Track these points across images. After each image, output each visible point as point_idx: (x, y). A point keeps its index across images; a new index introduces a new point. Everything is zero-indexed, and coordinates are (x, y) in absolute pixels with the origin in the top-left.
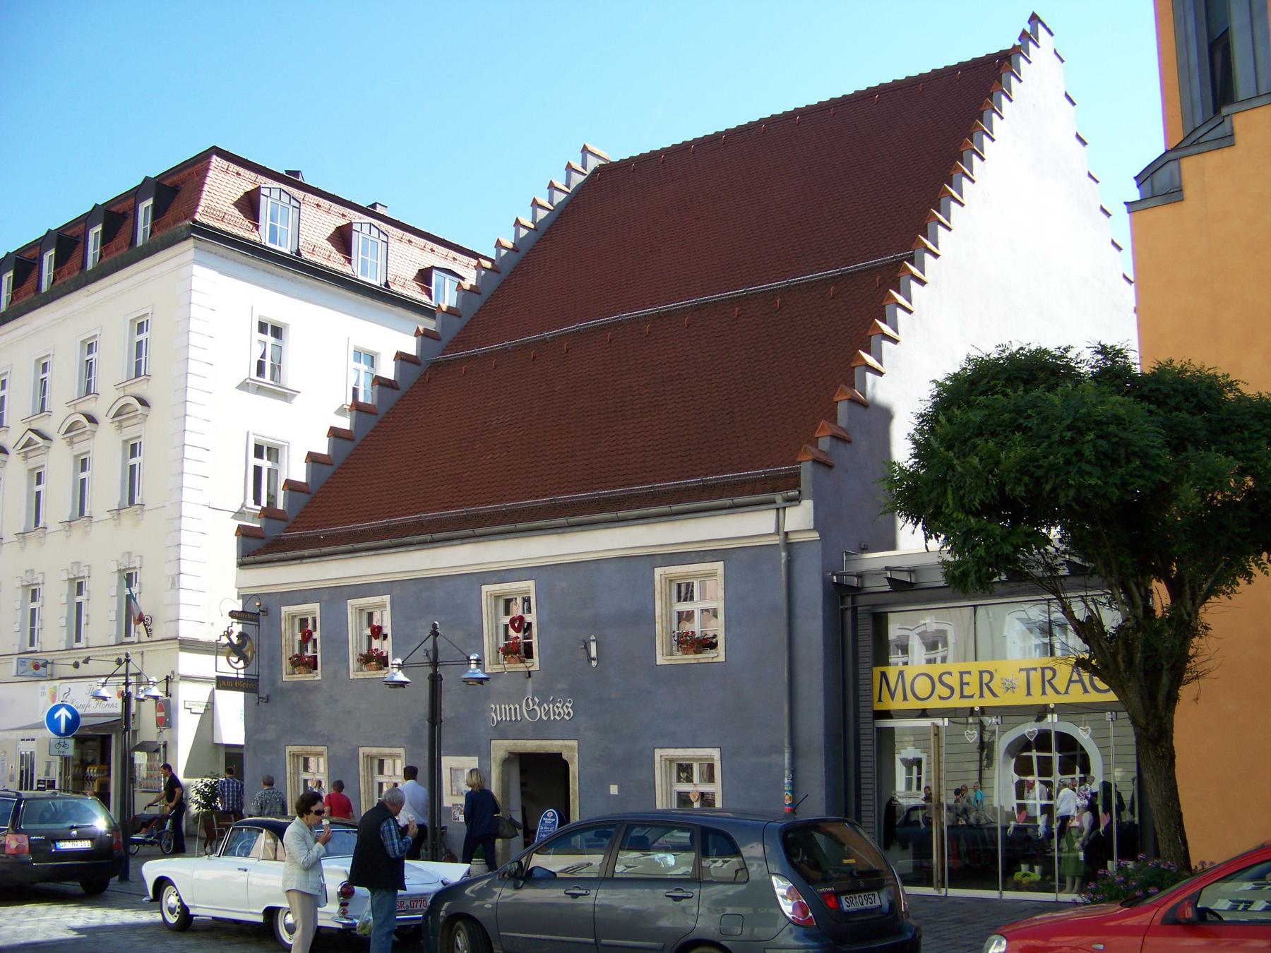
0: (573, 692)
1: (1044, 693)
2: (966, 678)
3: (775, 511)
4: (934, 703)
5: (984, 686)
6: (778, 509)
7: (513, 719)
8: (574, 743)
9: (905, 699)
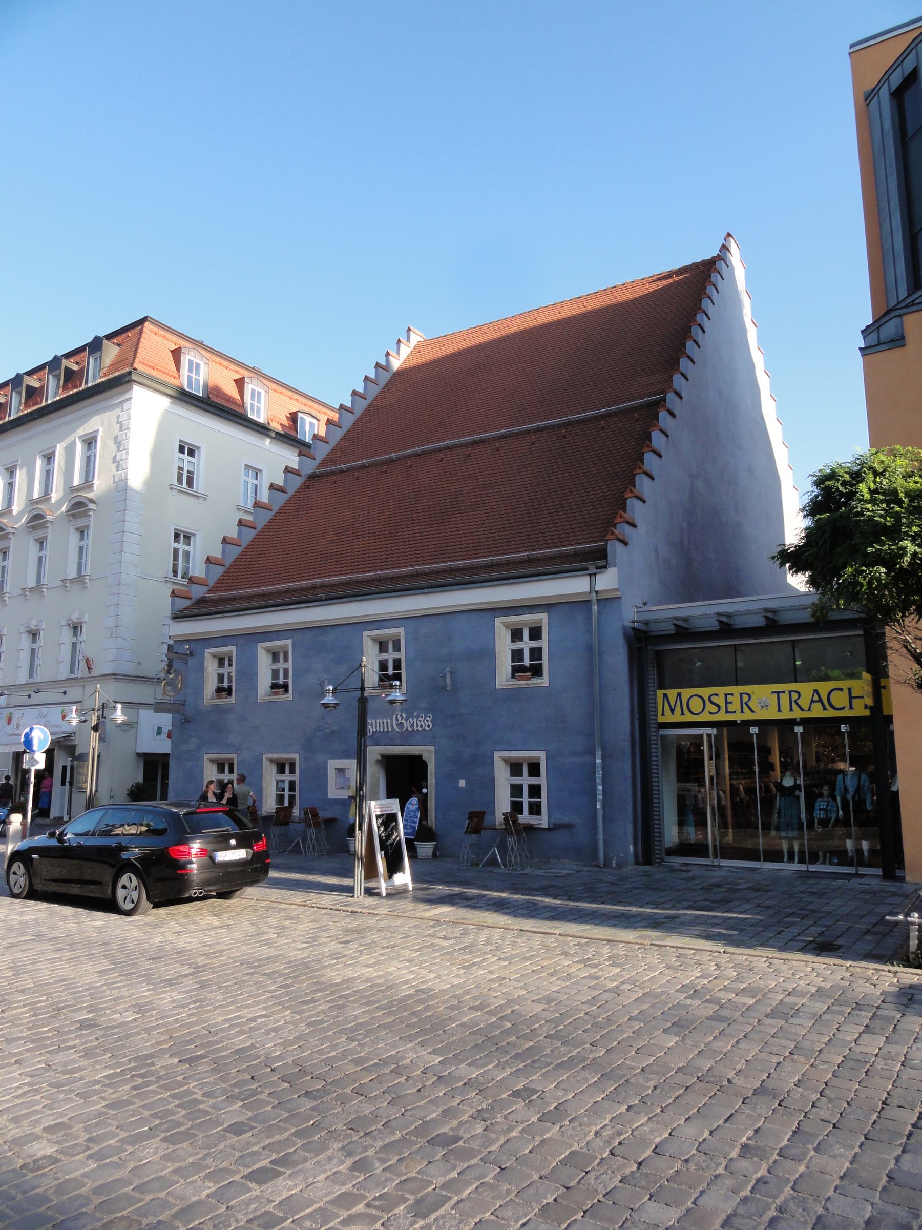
0: (432, 709)
1: (791, 710)
2: (730, 698)
3: (588, 577)
4: (705, 717)
5: (744, 705)
6: (590, 575)
7: (386, 730)
8: (432, 748)
9: (683, 714)
